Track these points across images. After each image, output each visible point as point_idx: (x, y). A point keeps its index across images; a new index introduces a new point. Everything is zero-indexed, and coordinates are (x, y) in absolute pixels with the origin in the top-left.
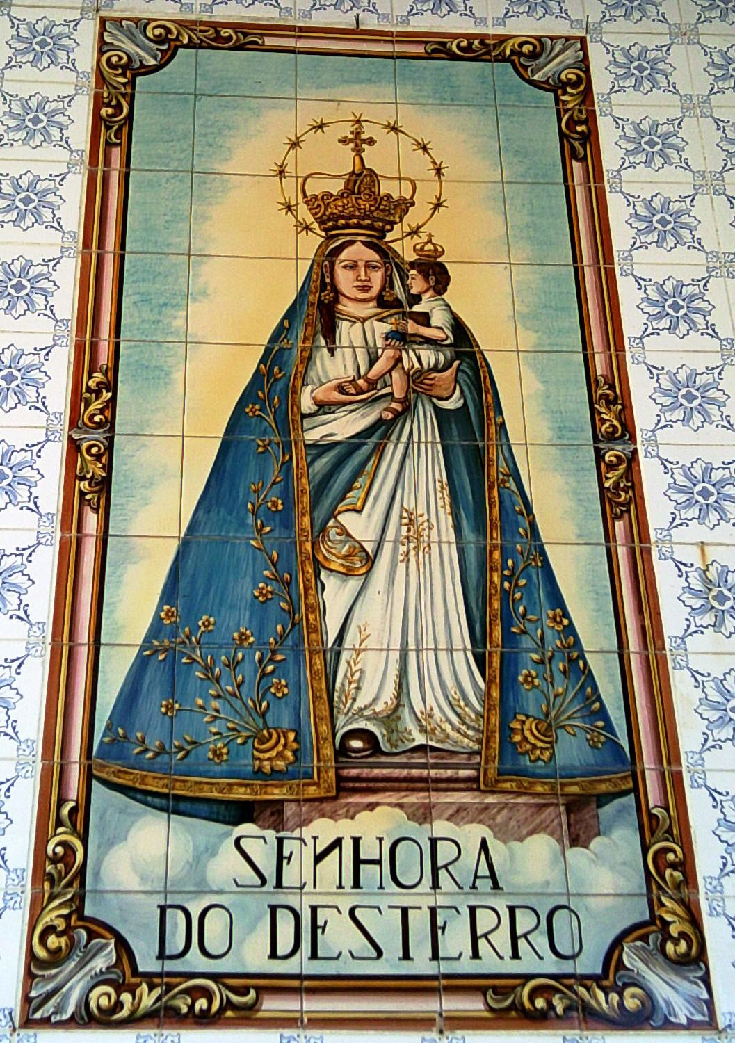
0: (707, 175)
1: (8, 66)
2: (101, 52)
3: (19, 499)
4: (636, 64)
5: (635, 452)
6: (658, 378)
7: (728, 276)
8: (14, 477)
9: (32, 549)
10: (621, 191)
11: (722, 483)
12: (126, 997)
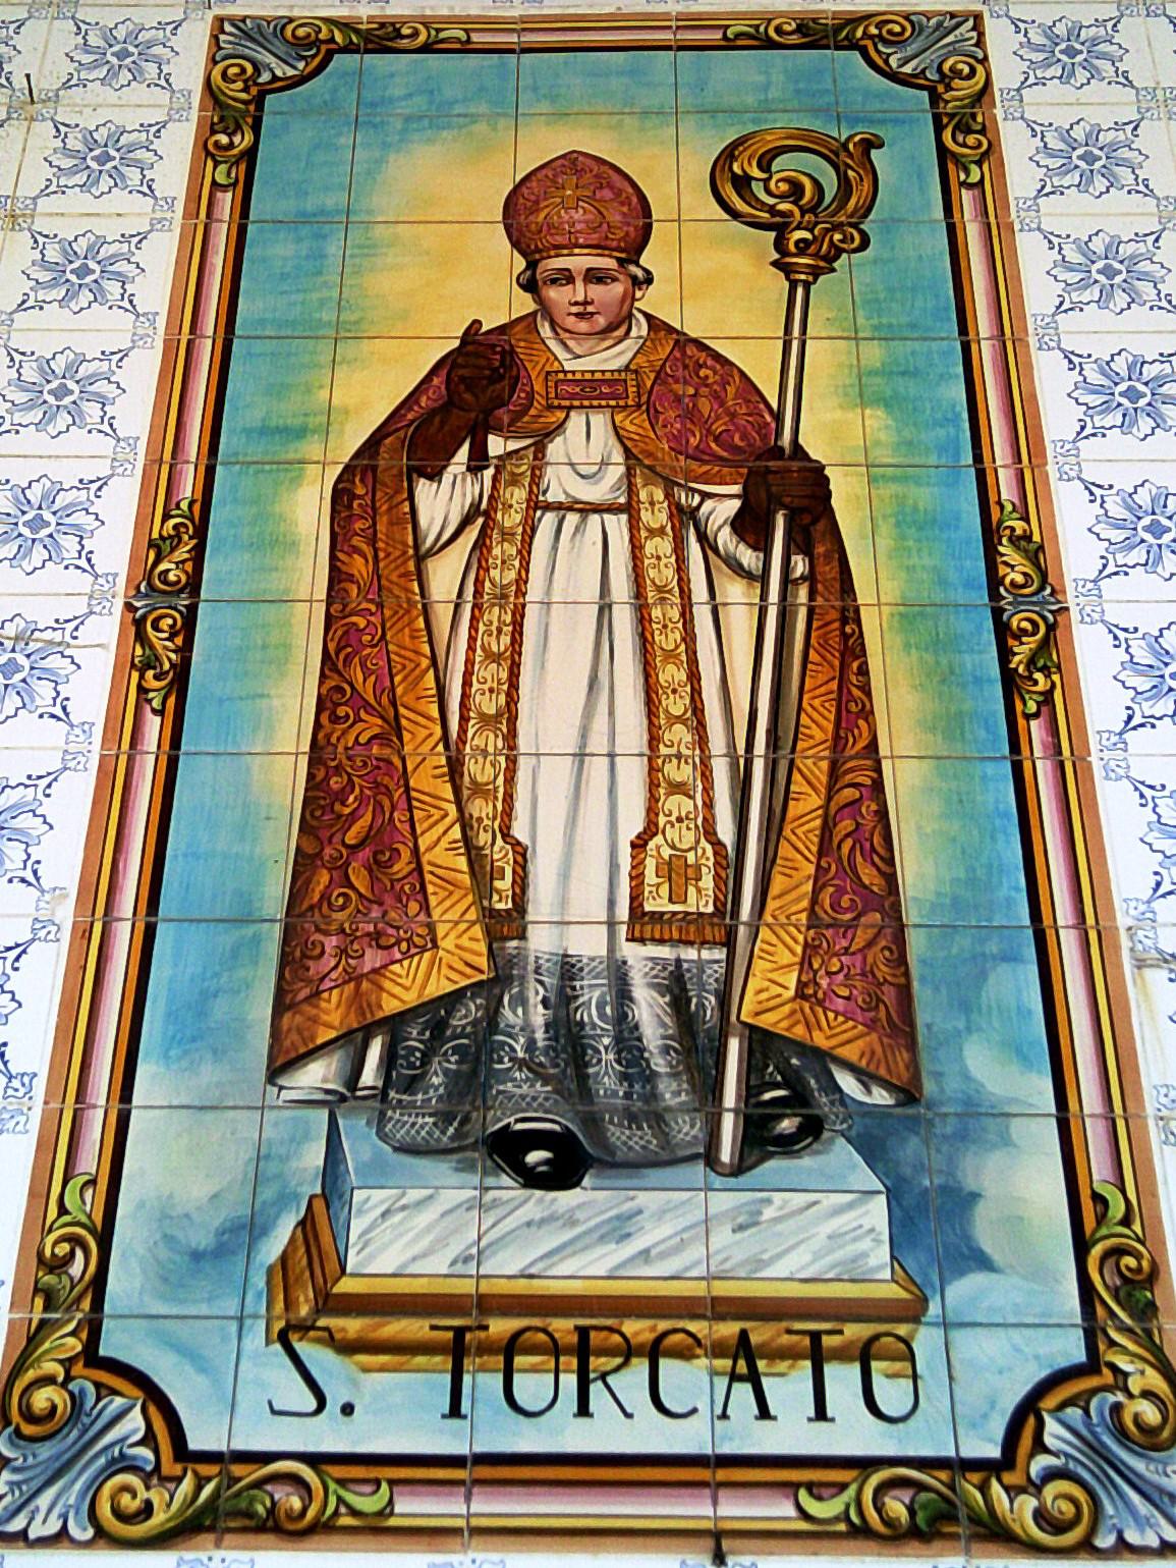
0: (1159, 93)
1: (22, 306)
3: (38, 701)
4: (1100, 264)
6: (1103, 502)
7: (1148, 15)
8: (32, 668)
9: (53, 777)
10: (1039, 229)
11: (1160, 381)
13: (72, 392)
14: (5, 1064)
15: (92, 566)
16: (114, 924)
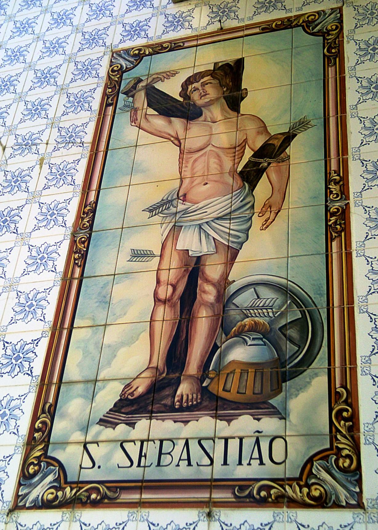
2: (111, 66)
5: (348, 205)
12: (60, 494)
13: (371, 50)
14: (376, 448)
15: (366, 259)
16: (338, 251)
